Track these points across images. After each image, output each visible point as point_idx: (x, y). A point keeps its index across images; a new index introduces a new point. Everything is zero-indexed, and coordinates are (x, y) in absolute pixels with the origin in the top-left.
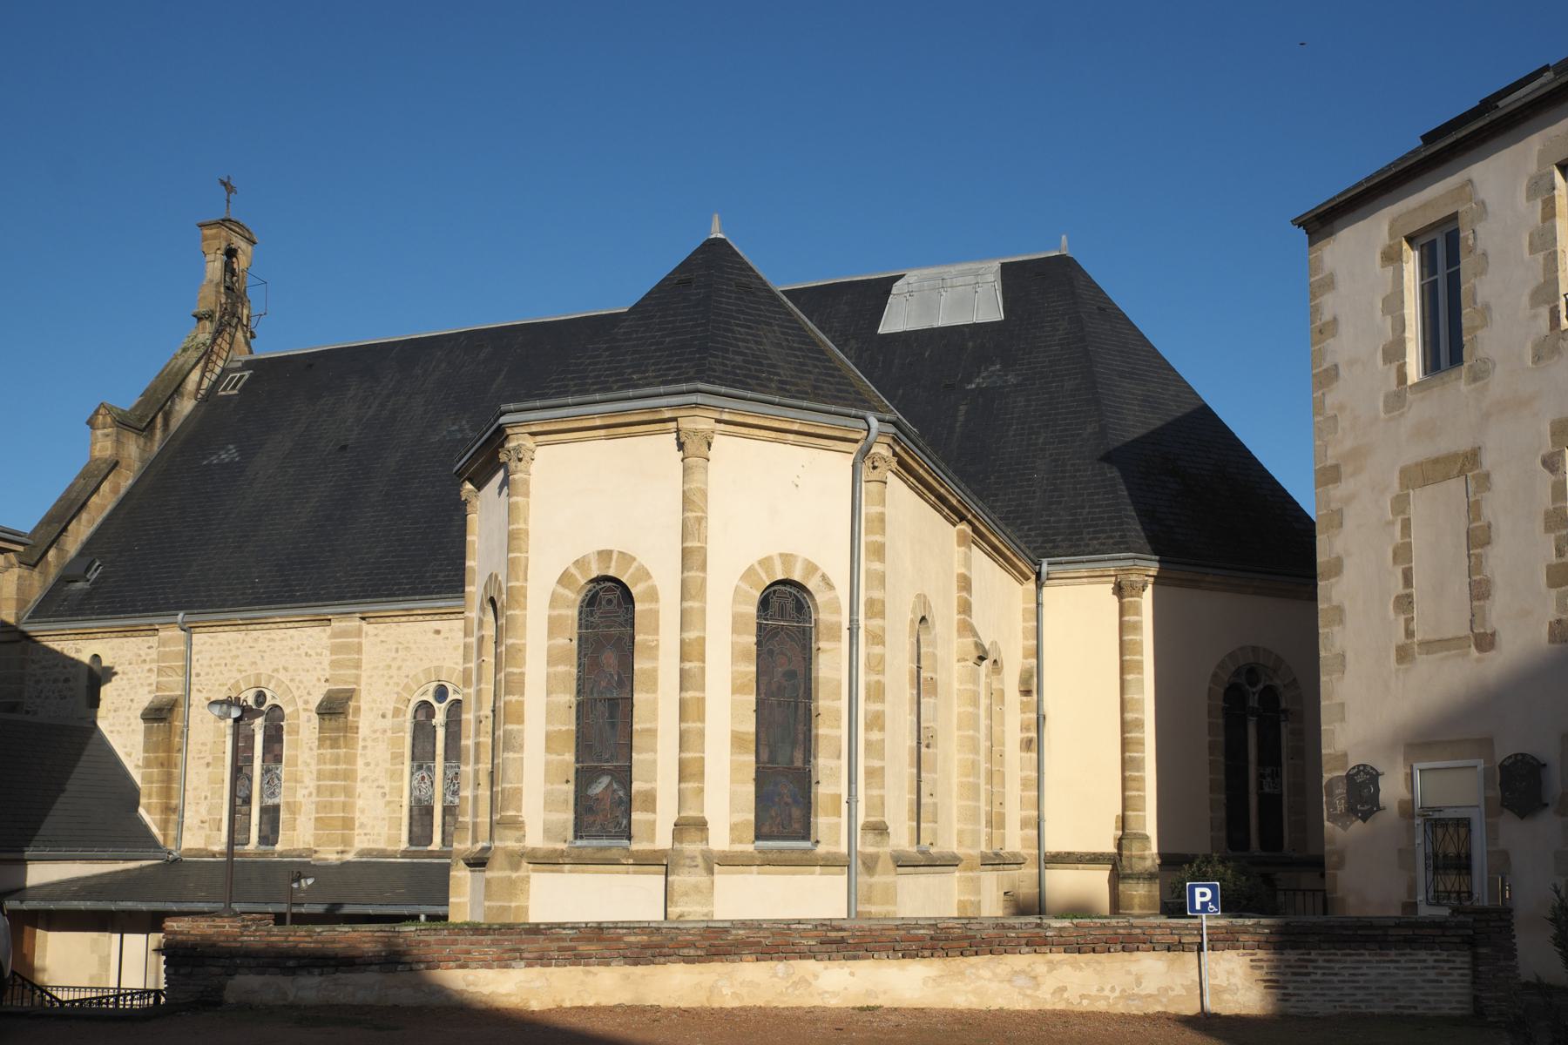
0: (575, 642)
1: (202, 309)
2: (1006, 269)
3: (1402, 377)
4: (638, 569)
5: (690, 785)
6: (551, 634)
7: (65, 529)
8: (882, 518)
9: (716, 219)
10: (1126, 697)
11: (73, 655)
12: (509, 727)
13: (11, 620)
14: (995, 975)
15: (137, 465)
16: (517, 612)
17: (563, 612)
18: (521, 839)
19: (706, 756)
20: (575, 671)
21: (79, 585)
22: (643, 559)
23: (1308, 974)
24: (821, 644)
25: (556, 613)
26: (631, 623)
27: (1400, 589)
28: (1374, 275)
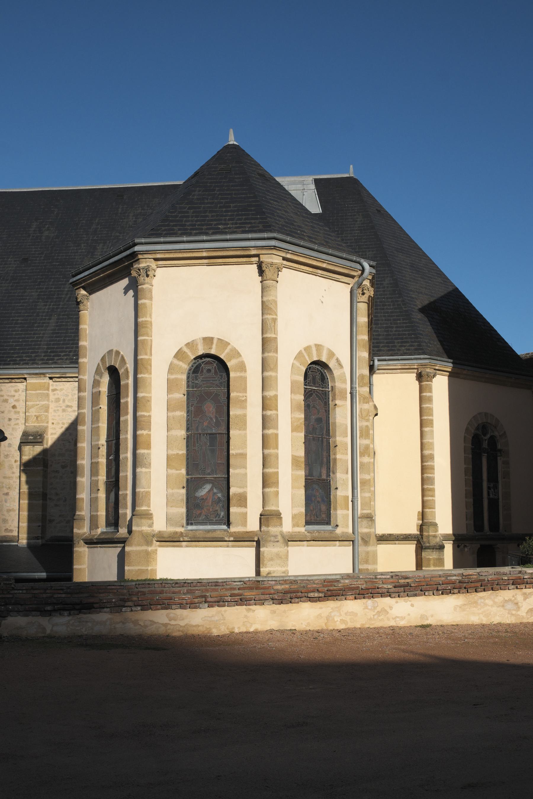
6: (170, 390)
9: (231, 132)
10: (425, 441)
14: (495, 603)
16: (146, 376)
17: (179, 376)
18: (151, 526)
22: (236, 343)
24: (337, 402)
25: (173, 377)
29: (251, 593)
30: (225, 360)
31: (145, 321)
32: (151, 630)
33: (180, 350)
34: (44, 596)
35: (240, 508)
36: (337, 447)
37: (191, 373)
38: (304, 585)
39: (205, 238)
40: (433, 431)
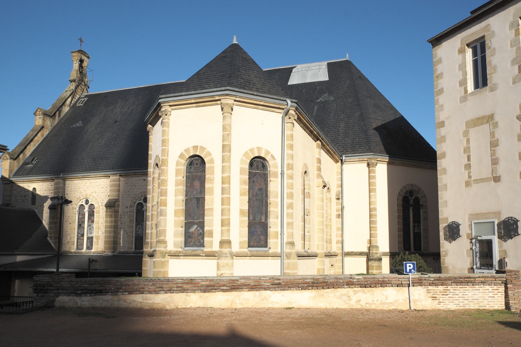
0: (185, 178)
1: (72, 78)
2: (329, 64)
3: (466, 91)
4: (207, 152)
5: (225, 228)
6: (177, 175)
7: (25, 148)
8: (292, 136)
11: (27, 188)
13: (7, 177)
15: (50, 128)
19: (231, 218)
20: (185, 188)
21: (29, 166)
22: (209, 149)
23: (447, 295)
24: (271, 179)
25: (178, 168)
26: (204, 171)
27: (466, 162)
28: (453, 58)
32: (133, 305)
34: (77, 285)
40: (376, 195)
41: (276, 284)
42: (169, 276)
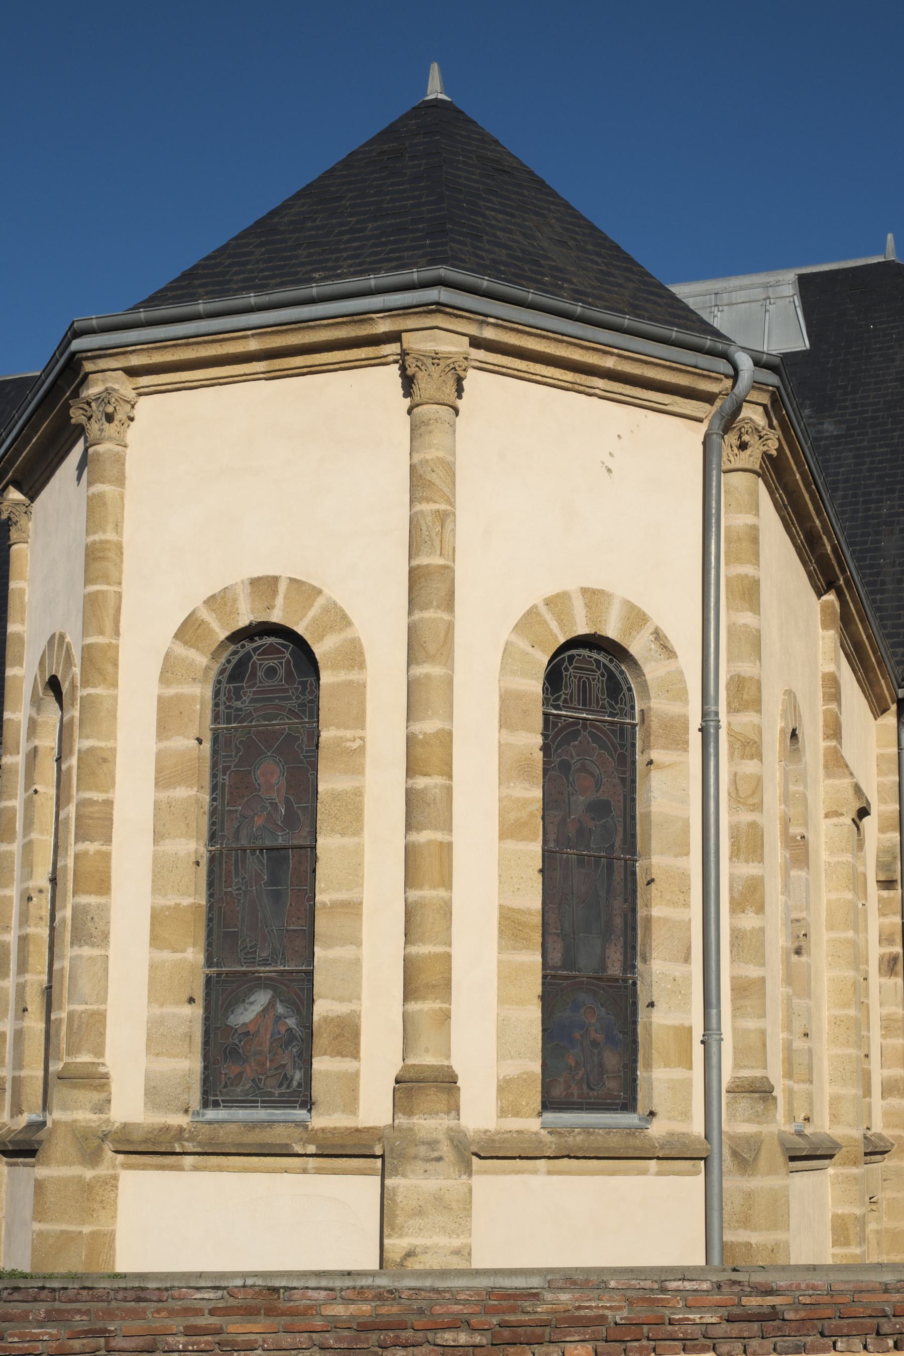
0: (207, 745)
2: (804, 282)
4: (326, 610)
5: (424, 1006)
6: (163, 729)
12: (84, 899)
20: (206, 798)
22: (337, 590)
25: (171, 691)
26: (310, 708)
29: (250, 1327)
30: (307, 637)
31: (101, 542)
33: (190, 615)
35: (339, 1058)
36: (653, 885)
37: (224, 680)
38: (424, 1304)
39: (253, 299)
41: (749, 1318)
42: (121, 1267)
